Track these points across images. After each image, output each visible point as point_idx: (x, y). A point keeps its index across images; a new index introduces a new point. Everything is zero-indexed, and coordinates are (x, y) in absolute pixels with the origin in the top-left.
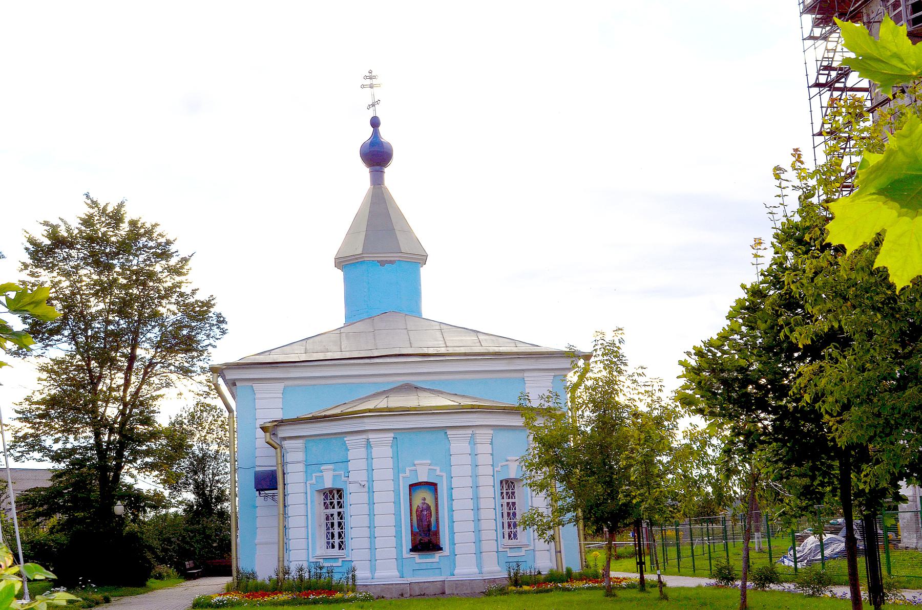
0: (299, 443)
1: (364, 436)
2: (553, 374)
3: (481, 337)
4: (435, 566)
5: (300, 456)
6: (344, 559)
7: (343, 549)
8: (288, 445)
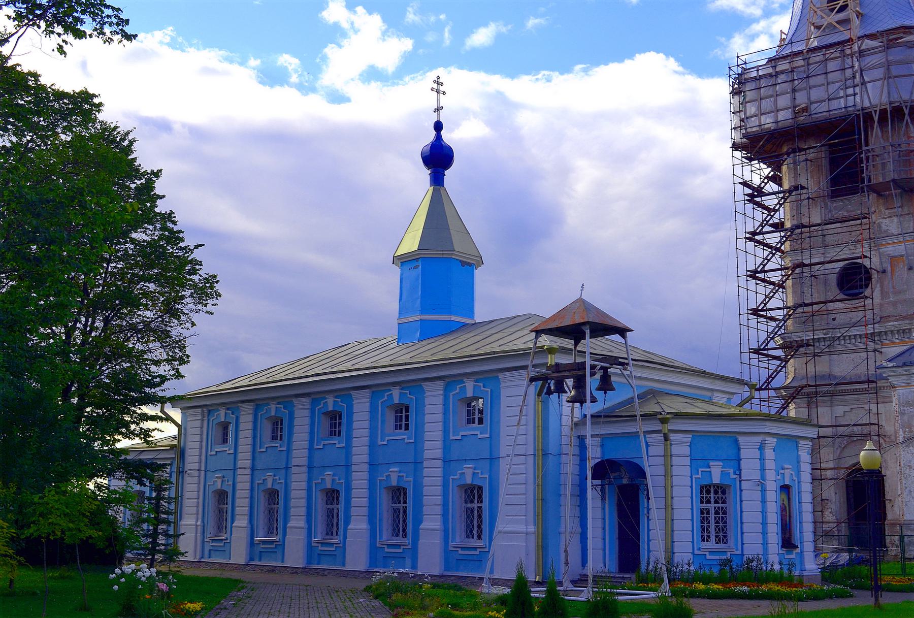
0: (688, 438)
1: (760, 438)
2: (727, 397)
3: (866, 361)
4: (475, 558)
5: (686, 450)
6: (405, 547)
7: (725, 543)
8: (675, 438)
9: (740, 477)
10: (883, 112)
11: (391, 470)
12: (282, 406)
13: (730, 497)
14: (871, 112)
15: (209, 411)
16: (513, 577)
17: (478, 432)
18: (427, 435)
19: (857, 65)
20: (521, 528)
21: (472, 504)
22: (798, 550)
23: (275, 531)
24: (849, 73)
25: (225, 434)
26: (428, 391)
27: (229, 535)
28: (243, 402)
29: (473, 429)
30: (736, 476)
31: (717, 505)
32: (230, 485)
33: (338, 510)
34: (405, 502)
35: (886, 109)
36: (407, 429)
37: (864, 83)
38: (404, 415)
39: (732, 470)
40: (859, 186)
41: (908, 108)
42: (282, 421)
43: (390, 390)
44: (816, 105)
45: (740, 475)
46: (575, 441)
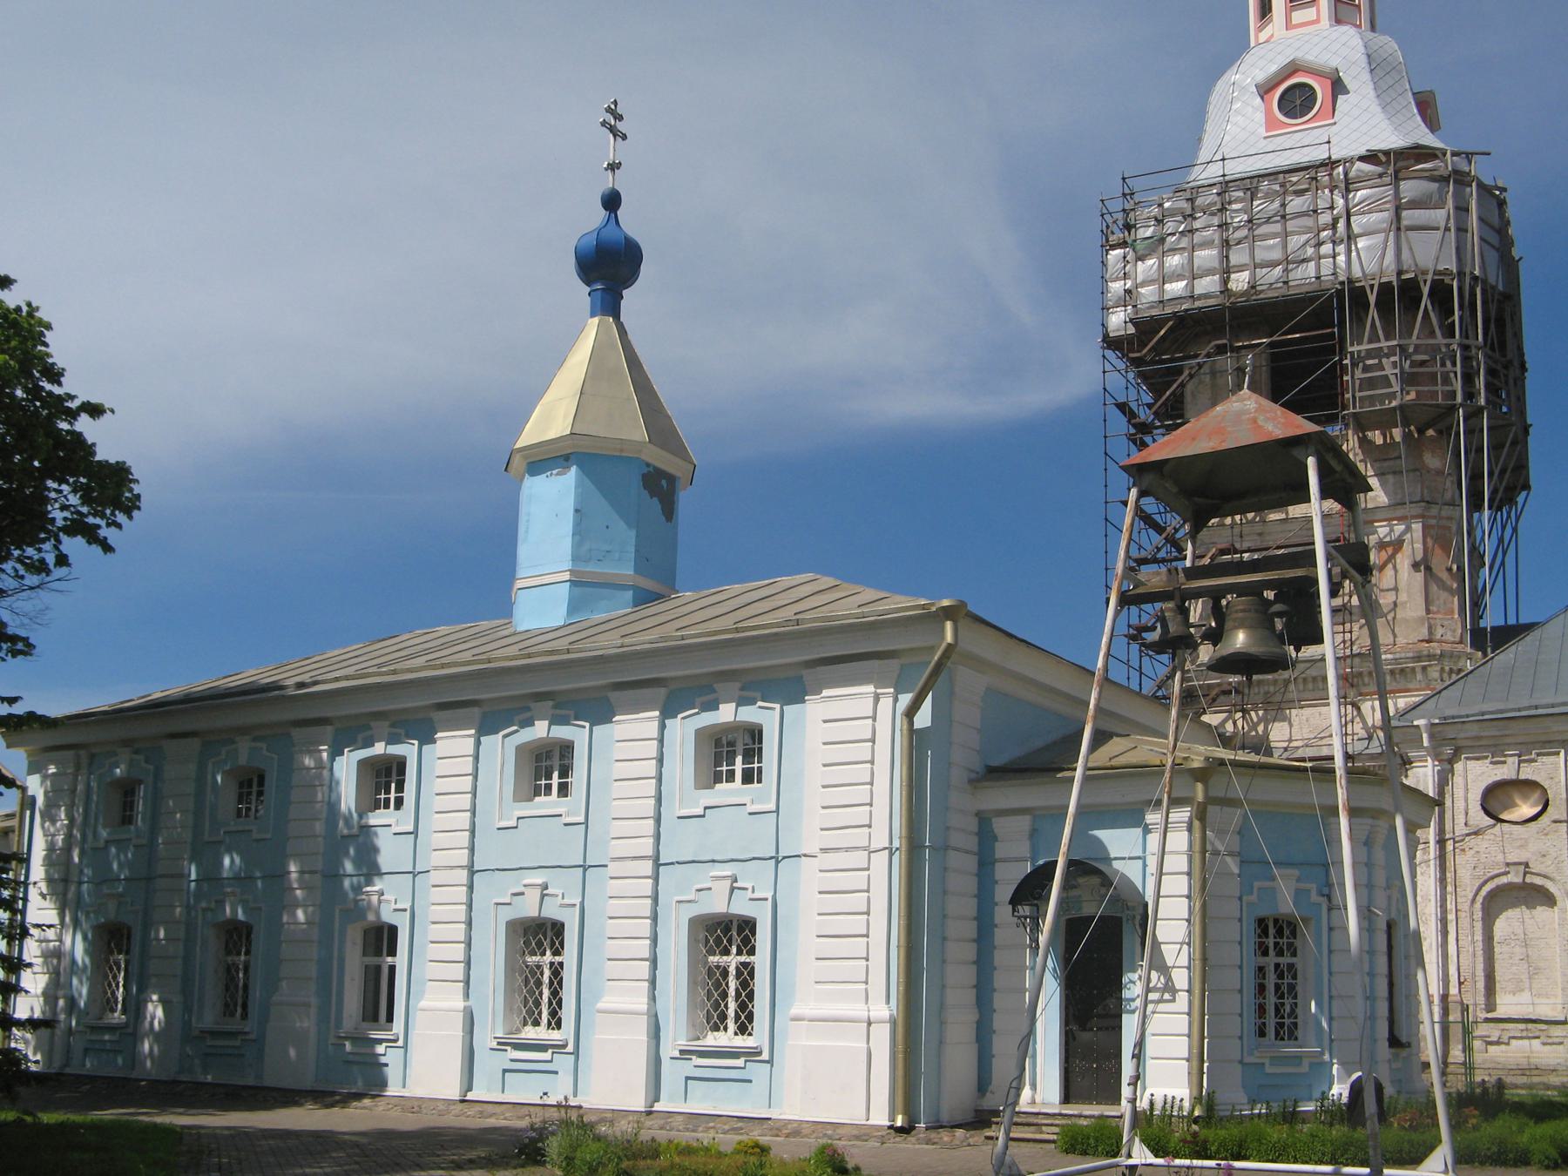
9: (1330, 900)
10: (1385, 289)
12: (264, 746)
13: (1307, 937)
14: (1363, 287)
15: (92, 757)
16: (22, 985)
19: (1340, 202)
20: (858, 1010)
21: (725, 958)
23: (239, 1010)
24: (1325, 218)
25: (128, 806)
28: (173, 736)
30: (1321, 899)
31: (1280, 960)
33: (392, 969)
35: (1390, 283)
37: (1351, 238)
39: (1314, 886)
40: (1337, 414)
41: (1428, 283)
42: (261, 782)
43: (528, 709)
44: (1265, 270)
45: (1329, 897)
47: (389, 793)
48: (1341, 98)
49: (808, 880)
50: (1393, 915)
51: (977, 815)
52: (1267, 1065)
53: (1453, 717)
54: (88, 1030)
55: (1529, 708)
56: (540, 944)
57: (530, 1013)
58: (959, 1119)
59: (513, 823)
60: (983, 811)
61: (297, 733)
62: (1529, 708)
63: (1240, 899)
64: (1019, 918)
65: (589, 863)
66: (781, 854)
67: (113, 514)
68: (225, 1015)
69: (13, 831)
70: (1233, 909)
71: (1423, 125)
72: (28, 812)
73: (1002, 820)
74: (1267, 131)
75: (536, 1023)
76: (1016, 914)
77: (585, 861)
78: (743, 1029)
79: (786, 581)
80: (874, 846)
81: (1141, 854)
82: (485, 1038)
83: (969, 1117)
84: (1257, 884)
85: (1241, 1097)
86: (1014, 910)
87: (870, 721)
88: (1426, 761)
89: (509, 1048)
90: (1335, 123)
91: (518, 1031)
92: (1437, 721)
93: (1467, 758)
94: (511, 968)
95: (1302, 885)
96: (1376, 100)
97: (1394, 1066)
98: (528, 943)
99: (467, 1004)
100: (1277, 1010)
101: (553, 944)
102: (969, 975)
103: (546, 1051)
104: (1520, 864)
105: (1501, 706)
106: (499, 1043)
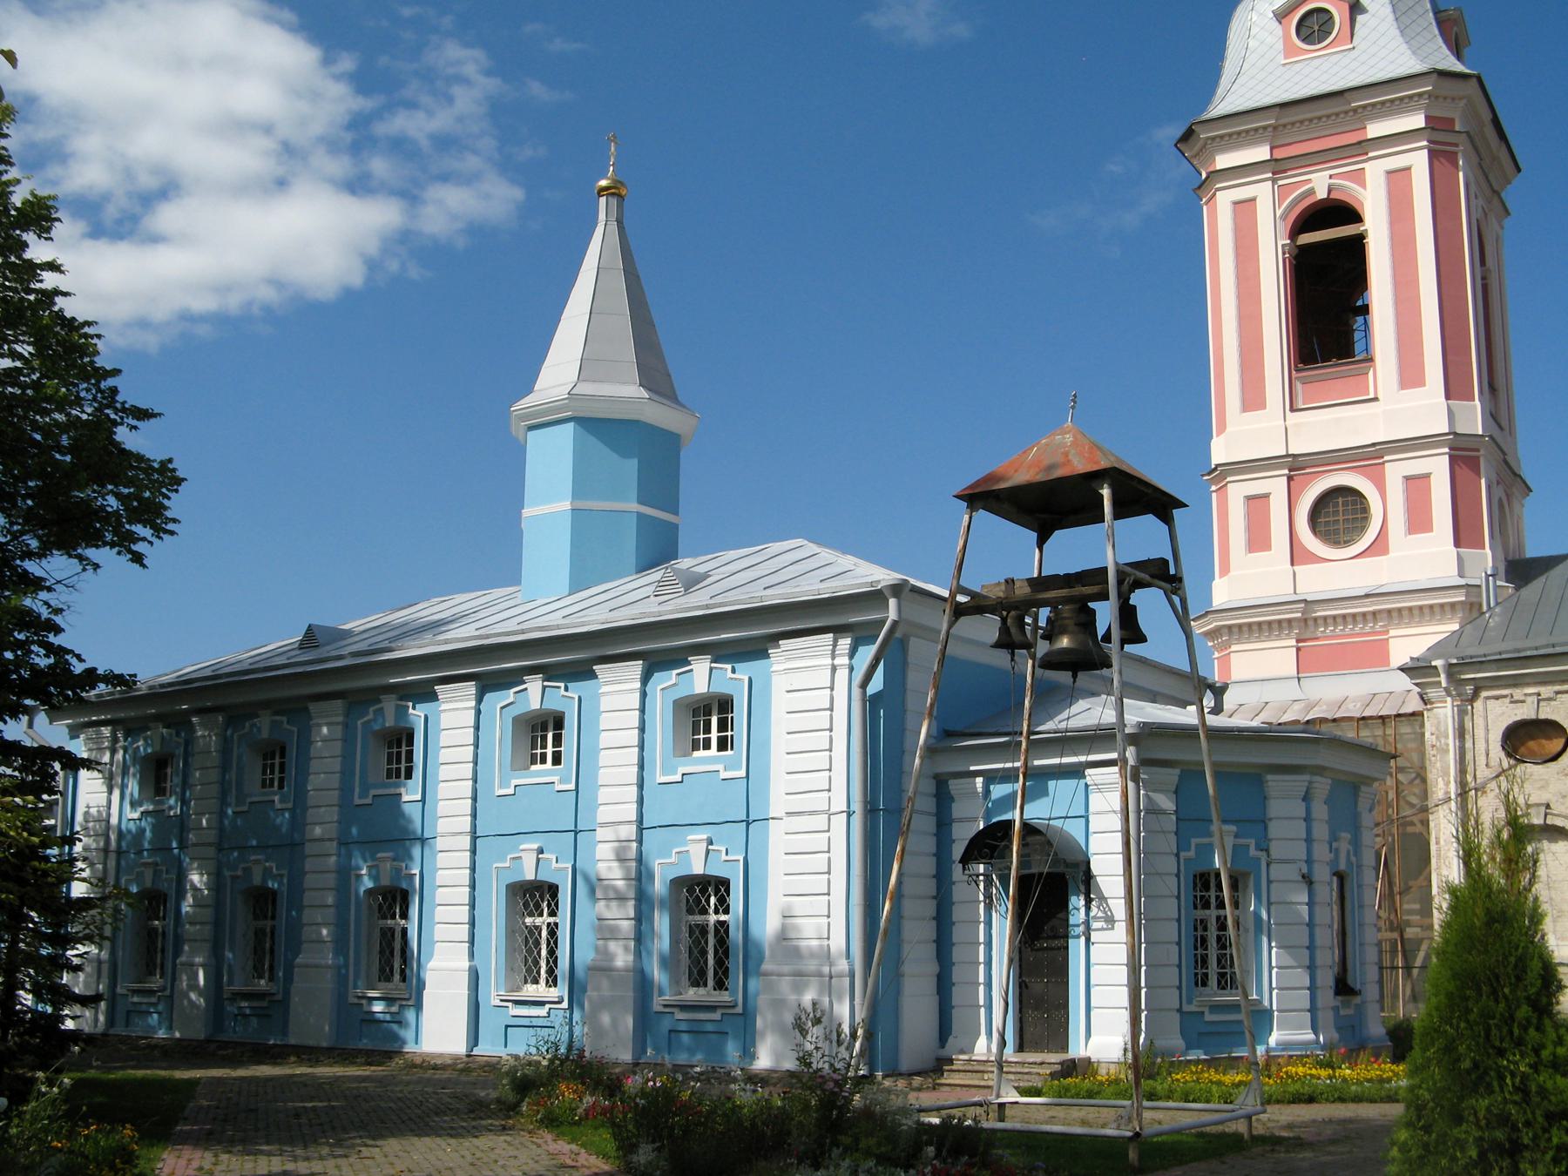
1: (1307, 777)
11: (379, 855)
12: (284, 719)
17: (720, 767)
18: (604, 776)
22: (1357, 1000)
26: (607, 683)
27: (169, 979)
29: (539, 774)
30: (1260, 853)
32: (172, 880)
34: (273, 918)
36: (557, 759)
38: (277, 761)
39: (1253, 841)
43: (379, 701)
46: (930, 787)
47: (400, 763)
48: (1360, 18)
49: (778, 839)
50: (1342, 866)
51: (934, 778)
52: (1207, 1013)
53: (1471, 657)
54: (130, 993)
55: (1547, 646)
56: (538, 907)
57: (529, 971)
58: (918, 1066)
59: (511, 791)
60: (941, 774)
61: (313, 707)
62: (1547, 646)
63: (1177, 855)
64: (970, 876)
65: (579, 828)
66: (751, 818)
67: (75, 693)
68: (1195, 907)
69: (57, 804)
70: (1170, 865)
71: (1444, 46)
72: (71, 781)
73: (956, 781)
74: (1285, 58)
75: (536, 981)
76: (966, 872)
77: (576, 827)
78: (720, 985)
79: (776, 547)
80: (833, 810)
81: (1083, 814)
82: (493, 994)
83: (931, 1064)
84: (1194, 841)
85: (1178, 1042)
86: (964, 869)
87: (828, 691)
88: (1446, 702)
89: (510, 1004)
90: (1354, 48)
91: (519, 989)
92: (1455, 661)
93: (1488, 698)
94: (511, 932)
95: (1241, 841)
96: (1395, 23)
97: (1342, 1012)
98: (526, 905)
99: (473, 963)
100: (1219, 961)
101: (549, 905)
102: (929, 930)
103: (715, 1012)
104: (1542, 804)
105: (1519, 645)
106: (502, 1000)
